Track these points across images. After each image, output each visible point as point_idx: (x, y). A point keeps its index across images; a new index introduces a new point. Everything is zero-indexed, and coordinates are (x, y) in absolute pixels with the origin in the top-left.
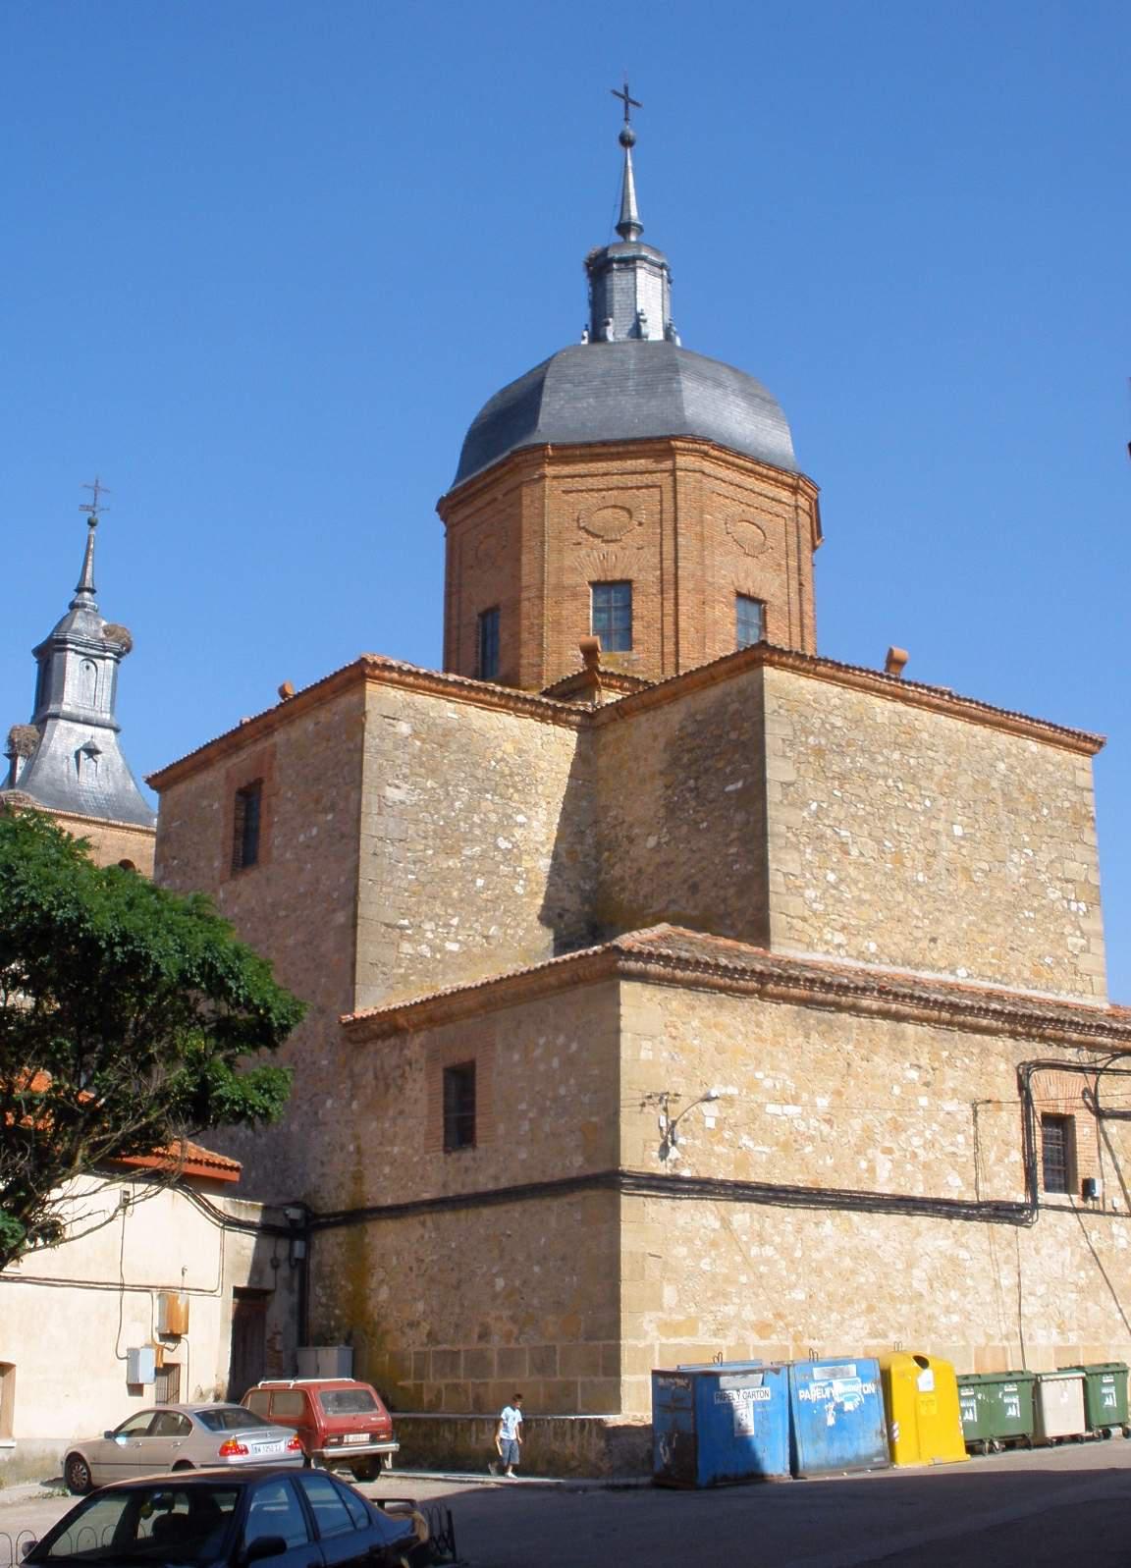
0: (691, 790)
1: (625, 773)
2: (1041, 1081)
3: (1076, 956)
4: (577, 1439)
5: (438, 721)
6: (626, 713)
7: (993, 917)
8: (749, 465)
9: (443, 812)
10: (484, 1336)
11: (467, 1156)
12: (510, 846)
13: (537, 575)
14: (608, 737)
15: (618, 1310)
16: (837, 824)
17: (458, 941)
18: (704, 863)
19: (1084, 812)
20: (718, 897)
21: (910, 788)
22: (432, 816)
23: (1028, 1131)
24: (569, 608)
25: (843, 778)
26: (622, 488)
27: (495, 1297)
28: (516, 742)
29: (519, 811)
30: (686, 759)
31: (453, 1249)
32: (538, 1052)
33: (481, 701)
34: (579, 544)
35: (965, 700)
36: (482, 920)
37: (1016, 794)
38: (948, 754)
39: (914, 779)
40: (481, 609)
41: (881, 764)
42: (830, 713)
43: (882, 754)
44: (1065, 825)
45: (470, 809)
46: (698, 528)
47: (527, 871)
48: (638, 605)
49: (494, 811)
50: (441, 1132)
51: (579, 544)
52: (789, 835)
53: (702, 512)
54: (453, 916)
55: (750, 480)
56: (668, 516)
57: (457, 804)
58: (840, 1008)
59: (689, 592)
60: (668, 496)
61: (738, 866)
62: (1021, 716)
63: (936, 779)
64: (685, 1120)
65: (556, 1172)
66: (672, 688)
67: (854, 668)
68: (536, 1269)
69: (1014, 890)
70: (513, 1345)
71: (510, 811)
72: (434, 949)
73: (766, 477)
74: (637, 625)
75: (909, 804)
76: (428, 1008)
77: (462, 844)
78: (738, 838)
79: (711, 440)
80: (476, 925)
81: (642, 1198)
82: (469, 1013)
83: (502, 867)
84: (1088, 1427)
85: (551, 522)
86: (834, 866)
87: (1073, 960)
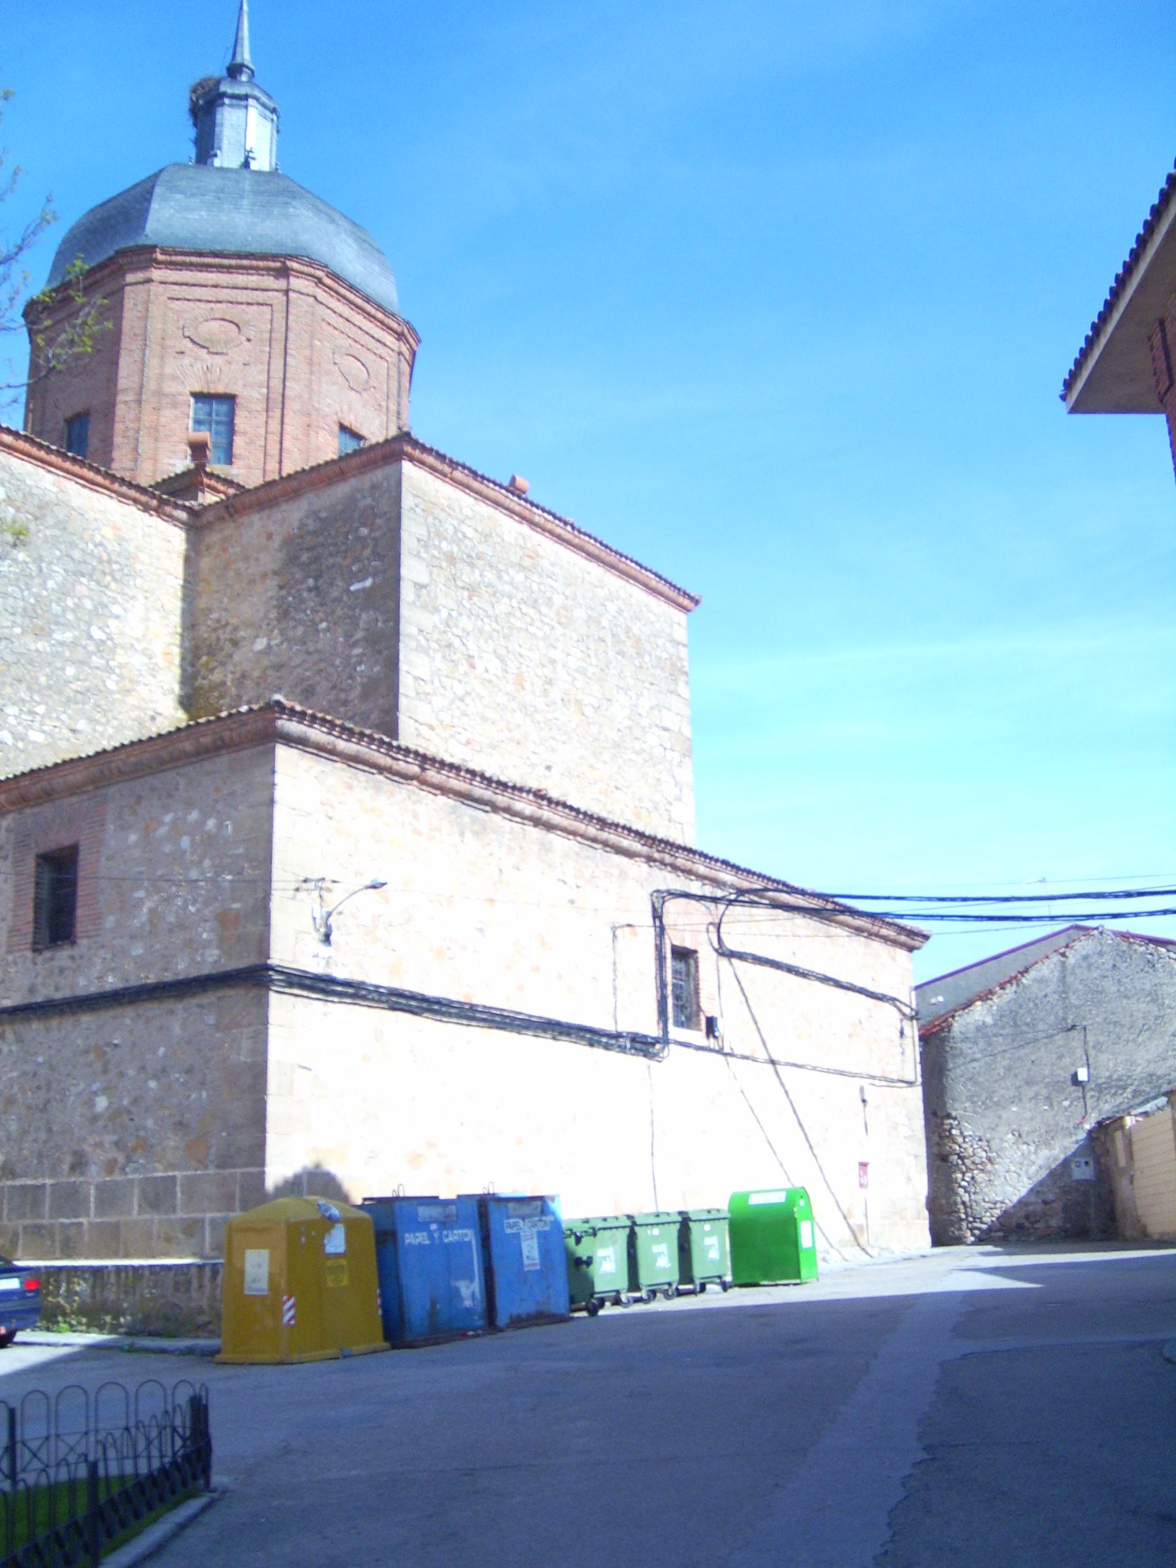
0: (310, 590)
1: (232, 573)
2: (673, 908)
3: (670, 803)
4: (207, 1290)
5: (35, 491)
6: (237, 511)
7: (601, 753)
8: (359, 301)
9: (34, 590)
10: (79, 1164)
11: (63, 955)
12: (104, 637)
13: (136, 379)
14: (214, 537)
15: (263, 1130)
16: (465, 634)
17: (43, 732)
18: (322, 665)
19: (679, 664)
20: (337, 700)
21: (532, 612)
22: (22, 591)
23: (661, 959)
24: (167, 415)
25: (472, 590)
26: (231, 302)
27: (95, 1118)
28: (115, 528)
29: (115, 602)
30: (305, 557)
31: (39, 1064)
32: (162, 831)
33: (81, 477)
34: (182, 353)
35: (585, 534)
36: (70, 712)
37: (623, 637)
38: (568, 585)
39: (535, 605)
40: (69, 414)
41: (506, 583)
42: (463, 522)
43: (508, 573)
44: (663, 675)
45: (63, 592)
46: (307, 352)
47: (120, 666)
48: (240, 421)
49: (89, 597)
50: (30, 928)
51: (182, 353)
52: (421, 638)
53: (312, 337)
54: (38, 703)
55: (358, 316)
56: (279, 335)
57: (51, 584)
58: (496, 808)
59: (294, 412)
60: (280, 316)
61: (363, 667)
62: (632, 561)
63: (555, 608)
64: (340, 913)
65: (182, 968)
66: (294, 483)
67: (489, 480)
68: (153, 1084)
69: (619, 730)
70: (117, 1177)
71: (105, 600)
72: (16, 737)
73: (373, 317)
74: (239, 441)
75: (530, 628)
76: (22, 784)
77: (53, 627)
78: (365, 638)
79: (326, 267)
80: (64, 717)
81: (292, 998)
82: (74, 790)
83: (94, 658)
84: (634, 1285)
85: (155, 326)
86: (461, 678)
87: (668, 807)
